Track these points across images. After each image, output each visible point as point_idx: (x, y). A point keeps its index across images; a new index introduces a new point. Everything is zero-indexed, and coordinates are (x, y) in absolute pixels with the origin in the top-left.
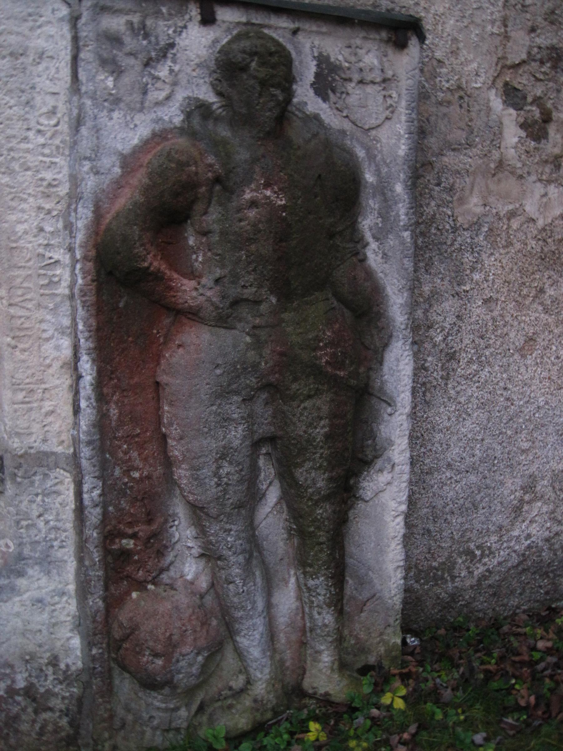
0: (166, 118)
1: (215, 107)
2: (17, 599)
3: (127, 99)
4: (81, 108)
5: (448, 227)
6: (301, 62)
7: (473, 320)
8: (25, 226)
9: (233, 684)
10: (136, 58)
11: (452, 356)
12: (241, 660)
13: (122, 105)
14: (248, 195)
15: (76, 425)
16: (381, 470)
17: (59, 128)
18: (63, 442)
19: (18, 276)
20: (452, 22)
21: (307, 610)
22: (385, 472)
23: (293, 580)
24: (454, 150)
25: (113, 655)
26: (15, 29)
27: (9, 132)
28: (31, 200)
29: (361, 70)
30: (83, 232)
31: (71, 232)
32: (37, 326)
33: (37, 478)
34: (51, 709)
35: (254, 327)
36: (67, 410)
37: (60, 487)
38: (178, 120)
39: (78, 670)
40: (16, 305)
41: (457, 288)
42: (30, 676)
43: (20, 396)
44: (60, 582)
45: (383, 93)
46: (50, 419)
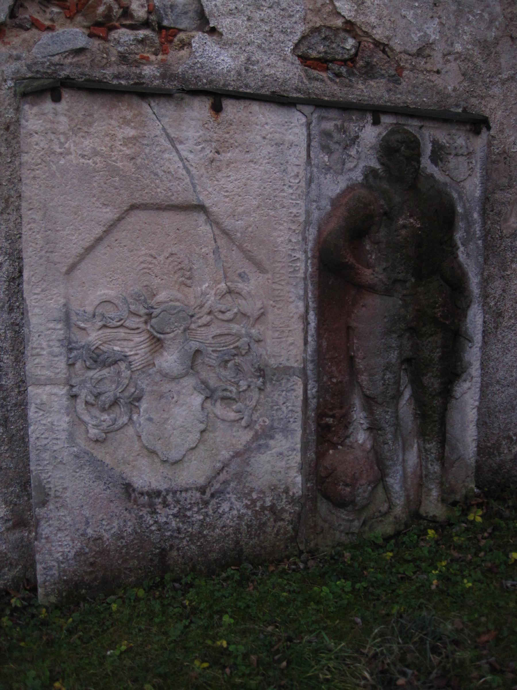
0: (354, 178)
1: (380, 171)
2: (269, 452)
3: (334, 168)
4: (311, 173)
5: (497, 236)
6: (424, 144)
7: (512, 292)
8: (282, 239)
9: (381, 509)
10: (340, 145)
11: (500, 315)
12: (386, 494)
13: (332, 171)
14: (401, 222)
15: (305, 351)
16: (465, 381)
17: (300, 184)
18: (298, 360)
19: (277, 267)
20: (500, 113)
21: (424, 463)
22: (467, 382)
23: (416, 446)
24: (501, 190)
25: (319, 487)
26: (278, 130)
27: (275, 187)
28: (285, 224)
29: (456, 148)
30: (312, 242)
31: (306, 242)
32: (287, 294)
33: (284, 381)
34: (283, 520)
35: (404, 295)
36: (301, 342)
37: (295, 387)
38: (360, 179)
39: (299, 496)
40: (276, 283)
41: (502, 273)
42: (273, 499)
43: (276, 334)
44: (293, 443)
45: (468, 160)
46: (291, 347)
